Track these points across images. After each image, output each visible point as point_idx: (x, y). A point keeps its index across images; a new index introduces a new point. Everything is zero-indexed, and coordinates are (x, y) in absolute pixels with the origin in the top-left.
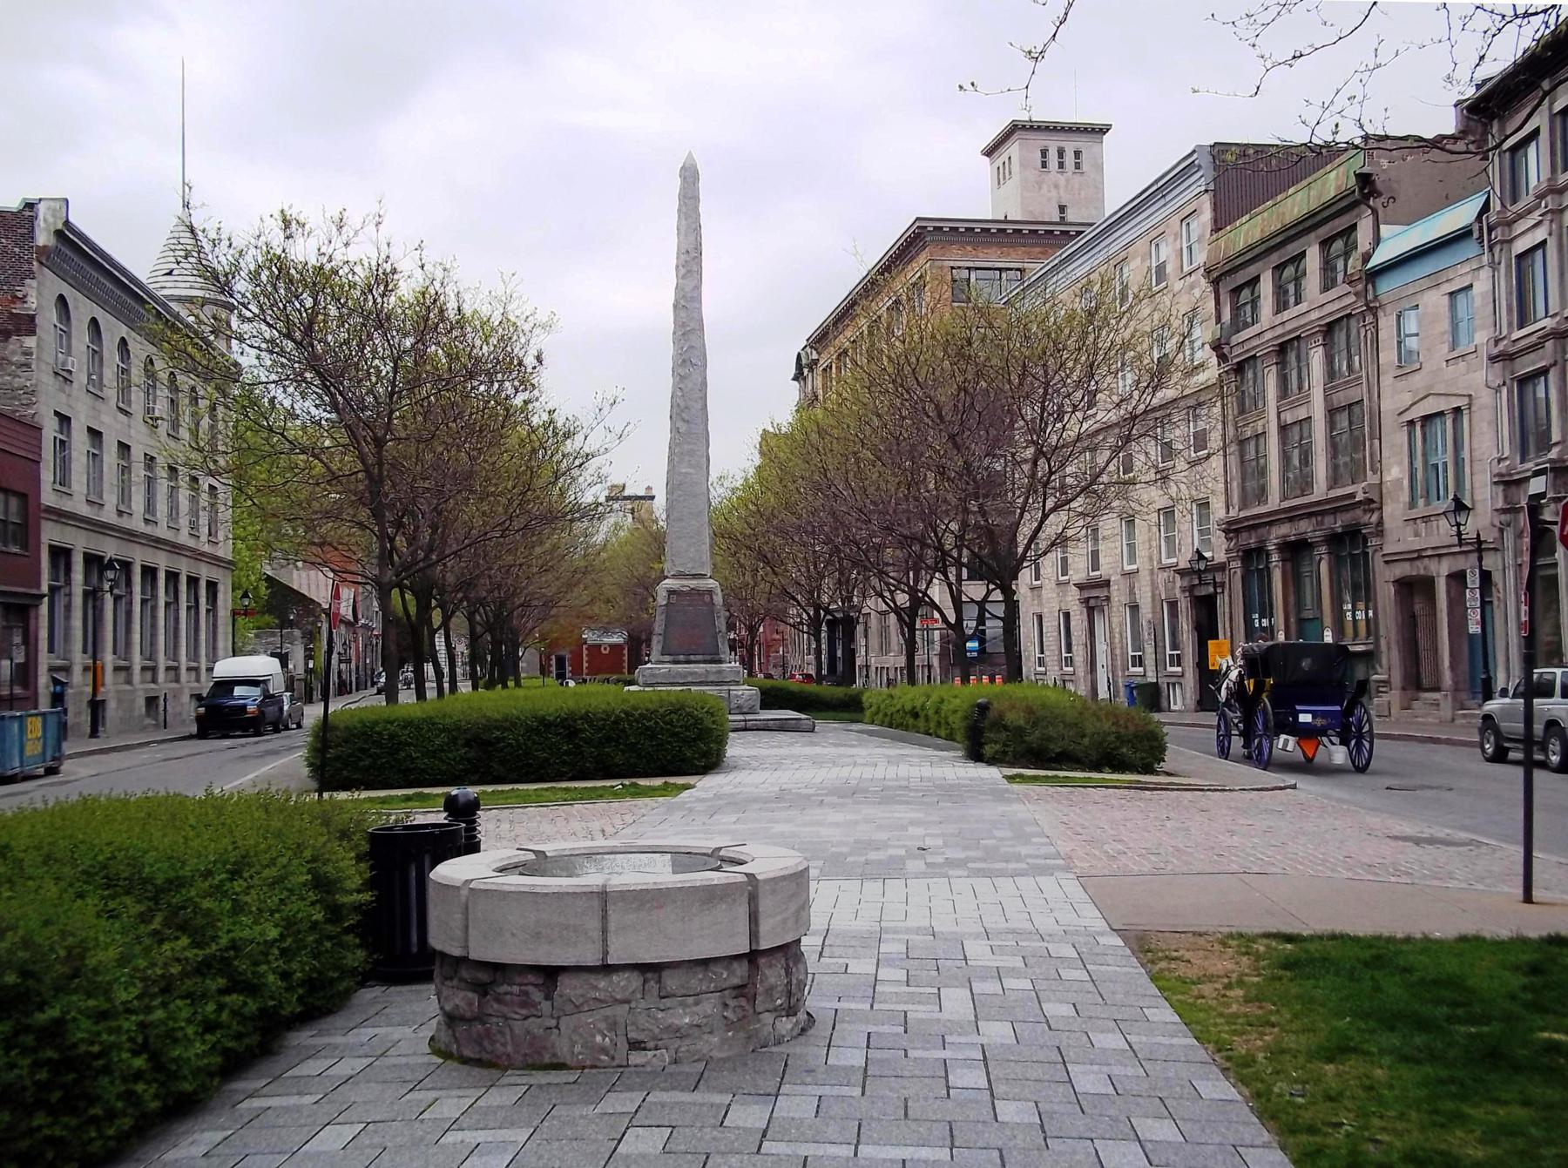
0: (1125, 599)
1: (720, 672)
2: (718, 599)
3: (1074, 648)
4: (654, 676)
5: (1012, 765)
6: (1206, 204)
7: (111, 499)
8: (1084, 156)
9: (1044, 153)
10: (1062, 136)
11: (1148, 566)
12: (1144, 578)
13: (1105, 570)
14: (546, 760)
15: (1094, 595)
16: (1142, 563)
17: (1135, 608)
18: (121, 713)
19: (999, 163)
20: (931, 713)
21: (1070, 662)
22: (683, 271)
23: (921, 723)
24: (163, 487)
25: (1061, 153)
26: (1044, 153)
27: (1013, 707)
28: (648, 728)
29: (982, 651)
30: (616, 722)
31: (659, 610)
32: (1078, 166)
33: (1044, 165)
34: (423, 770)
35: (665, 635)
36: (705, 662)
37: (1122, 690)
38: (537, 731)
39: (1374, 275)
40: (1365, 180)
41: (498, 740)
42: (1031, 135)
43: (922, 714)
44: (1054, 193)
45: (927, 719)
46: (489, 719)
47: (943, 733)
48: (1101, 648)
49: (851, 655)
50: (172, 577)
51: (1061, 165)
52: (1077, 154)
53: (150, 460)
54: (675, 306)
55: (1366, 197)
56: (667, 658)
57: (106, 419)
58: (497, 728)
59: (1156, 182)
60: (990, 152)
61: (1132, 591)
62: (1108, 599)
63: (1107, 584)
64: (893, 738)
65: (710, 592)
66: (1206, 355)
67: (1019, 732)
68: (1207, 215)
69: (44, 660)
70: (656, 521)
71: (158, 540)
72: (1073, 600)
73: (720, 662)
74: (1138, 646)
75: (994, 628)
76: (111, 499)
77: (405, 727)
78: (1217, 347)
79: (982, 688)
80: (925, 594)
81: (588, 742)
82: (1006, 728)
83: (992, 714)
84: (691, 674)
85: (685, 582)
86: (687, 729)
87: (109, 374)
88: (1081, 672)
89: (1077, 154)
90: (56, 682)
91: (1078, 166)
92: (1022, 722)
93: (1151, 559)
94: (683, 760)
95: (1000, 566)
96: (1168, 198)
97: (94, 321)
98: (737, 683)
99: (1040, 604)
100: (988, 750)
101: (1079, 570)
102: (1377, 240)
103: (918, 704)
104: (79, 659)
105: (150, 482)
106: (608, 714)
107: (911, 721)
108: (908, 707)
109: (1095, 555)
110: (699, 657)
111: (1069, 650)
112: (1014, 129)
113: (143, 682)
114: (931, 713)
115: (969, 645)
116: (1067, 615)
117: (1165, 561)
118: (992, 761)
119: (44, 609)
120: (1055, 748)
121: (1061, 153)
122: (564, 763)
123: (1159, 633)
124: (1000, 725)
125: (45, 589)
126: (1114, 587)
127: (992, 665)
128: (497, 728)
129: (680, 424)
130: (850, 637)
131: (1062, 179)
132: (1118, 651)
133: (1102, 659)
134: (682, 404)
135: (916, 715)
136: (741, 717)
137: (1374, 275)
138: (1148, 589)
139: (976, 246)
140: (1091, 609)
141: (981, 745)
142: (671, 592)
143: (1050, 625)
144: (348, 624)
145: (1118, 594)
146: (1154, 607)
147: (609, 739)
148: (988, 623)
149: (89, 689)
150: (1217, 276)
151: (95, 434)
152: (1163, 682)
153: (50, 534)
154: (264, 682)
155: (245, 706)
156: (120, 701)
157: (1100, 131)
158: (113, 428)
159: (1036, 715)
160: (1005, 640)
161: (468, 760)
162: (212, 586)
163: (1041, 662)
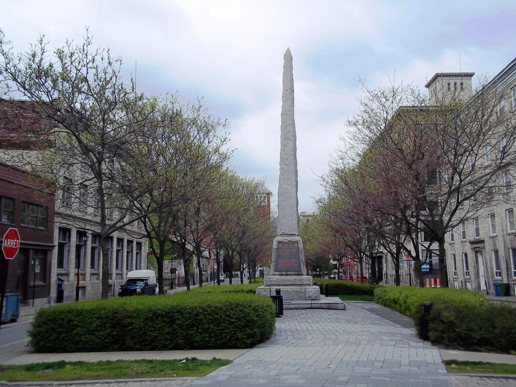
0: (492, 248)
1: (301, 280)
2: (301, 245)
3: (470, 268)
4: (271, 281)
5: (448, 347)
8: (464, 84)
11: (501, 234)
12: (500, 239)
13: (482, 237)
14: (157, 337)
15: (478, 246)
16: (499, 232)
17: (496, 252)
18: (92, 291)
19: (432, 89)
20: (402, 302)
21: (468, 274)
22: (285, 99)
23: (398, 306)
25: (455, 84)
27: (447, 308)
28: (216, 319)
29: (431, 269)
30: (197, 315)
31: (274, 251)
34: (86, 342)
35: (276, 262)
36: (295, 275)
37: (492, 286)
38: (151, 319)
41: (130, 324)
43: (398, 303)
45: (400, 305)
46: (127, 311)
47: (408, 313)
48: (482, 268)
49: (381, 269)
50: (130, 242)
52: (462, 84)
54: (282, 115)
56: (277, 273)
58: (130, 317)
59: (501, 72)
60: (428, 86)
61: (495, 244)
62: (484, 248)
63: (483, 242)
64: (384, 316)
65: (297, 242)
67: (451, 326)
69: (55, 270)
72: (468, 249)
73: (302, 275)
74: (498, 267)
75: (435, 260)
77: (78, 316)
79: (431, 290)
80: (402, 244)
81: (181, 326)
82: (443, 322)
83: (432, 312)
84: (288, 280)
85: (286, 238)
86: (239, 320)
88: (473, 278)
89: (462, 84)
90: (59, 280)
92: (452, 318)
93: (503, 231)
94: (237, 339)
95: (436, 233)
96: (504, 81)
98: (309, 285)
99: (454, 250)
100: (431, 334)
101: (471, 235)
103: (396, 297)
104: (73, 270)
106: (193, 309)
107: (393, 305)
108: (392, 298)
109: (477, 230)
110: (292, 273)
111: (467, 269)
112: (437, 76)
113: (116, 279)
114: (402, 302)
115: (424, 266)
116: (466, 255)
117: (509, 231)
118: (437, 342)
119: (56, 251)
120: (477, 335)
122: (166, 339)
123: (508, 262)
124: (438, 318)
125: (56, 243)
126: (486, 243)
127: (435, 274)
128: (130, 317)
129: (284, 166)
130: (380, 263)
132: (489, 270)
133: (482, 272)
134: (285, 158)
135: (396, 303)
136: (310, 302)
138: (502, 243)
140: (477, 252)
141: (427, 331)
142: (279, 242)
143: (459, 259)
144: (207, 258)
145: (488, 246)
146: (505, 251)
147: (193, 325)
148: (433, 258)
149: (76, 282)
152: (511, 283)
153: (58, 223)
154: (146, 280)
155: (136, 289)
156: (92, 287)
159: (463, 312)
160: (440, 265)
161: (113, 336)
162: (139, 244)
163: (455, 274)
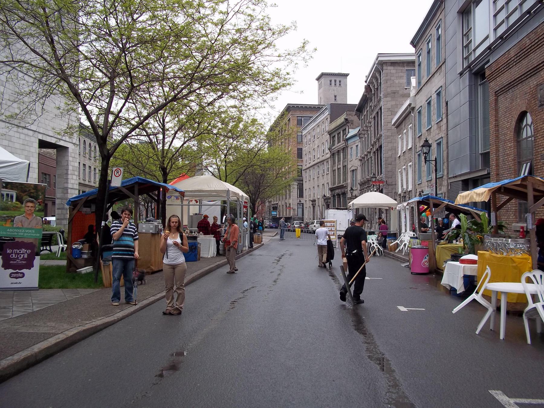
6: (329, 117)
7: (87, 179)
8: (342, 82)
9: (331, 81)
10: (335, 77)
24: (93, 173)
25: (335, 81)
26: (331, 81)
32: (340, 85)
33: (331, 84)
39: (347, 140)
40: (346, 120)
42: (327, 76)
44: (333, 92)
51: (335, 85)
52: (340, 81)
53: (90, 167)
55: (347, 123)
57: (86, 161)
60: (318, 79)
66: (327, 151)
68: (329, 119)
70: (145, 200)
71: (91, 186)
76: (87, 179)
78: (329, 149)
87: (87, 151)
89: (340, 81)
91: (340, 85)
97: (90, 144)
102: (349, 132)
105: (90, 172)
121: (335, 81)
131: (335, 88)
137: (347, 140)
139: (303, 111)
150: (330, 133)
151: (84, 165)
157: (346, 75)
158: (88, 163)
